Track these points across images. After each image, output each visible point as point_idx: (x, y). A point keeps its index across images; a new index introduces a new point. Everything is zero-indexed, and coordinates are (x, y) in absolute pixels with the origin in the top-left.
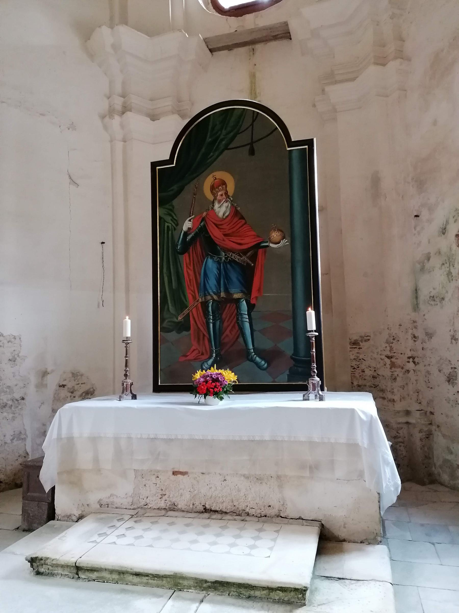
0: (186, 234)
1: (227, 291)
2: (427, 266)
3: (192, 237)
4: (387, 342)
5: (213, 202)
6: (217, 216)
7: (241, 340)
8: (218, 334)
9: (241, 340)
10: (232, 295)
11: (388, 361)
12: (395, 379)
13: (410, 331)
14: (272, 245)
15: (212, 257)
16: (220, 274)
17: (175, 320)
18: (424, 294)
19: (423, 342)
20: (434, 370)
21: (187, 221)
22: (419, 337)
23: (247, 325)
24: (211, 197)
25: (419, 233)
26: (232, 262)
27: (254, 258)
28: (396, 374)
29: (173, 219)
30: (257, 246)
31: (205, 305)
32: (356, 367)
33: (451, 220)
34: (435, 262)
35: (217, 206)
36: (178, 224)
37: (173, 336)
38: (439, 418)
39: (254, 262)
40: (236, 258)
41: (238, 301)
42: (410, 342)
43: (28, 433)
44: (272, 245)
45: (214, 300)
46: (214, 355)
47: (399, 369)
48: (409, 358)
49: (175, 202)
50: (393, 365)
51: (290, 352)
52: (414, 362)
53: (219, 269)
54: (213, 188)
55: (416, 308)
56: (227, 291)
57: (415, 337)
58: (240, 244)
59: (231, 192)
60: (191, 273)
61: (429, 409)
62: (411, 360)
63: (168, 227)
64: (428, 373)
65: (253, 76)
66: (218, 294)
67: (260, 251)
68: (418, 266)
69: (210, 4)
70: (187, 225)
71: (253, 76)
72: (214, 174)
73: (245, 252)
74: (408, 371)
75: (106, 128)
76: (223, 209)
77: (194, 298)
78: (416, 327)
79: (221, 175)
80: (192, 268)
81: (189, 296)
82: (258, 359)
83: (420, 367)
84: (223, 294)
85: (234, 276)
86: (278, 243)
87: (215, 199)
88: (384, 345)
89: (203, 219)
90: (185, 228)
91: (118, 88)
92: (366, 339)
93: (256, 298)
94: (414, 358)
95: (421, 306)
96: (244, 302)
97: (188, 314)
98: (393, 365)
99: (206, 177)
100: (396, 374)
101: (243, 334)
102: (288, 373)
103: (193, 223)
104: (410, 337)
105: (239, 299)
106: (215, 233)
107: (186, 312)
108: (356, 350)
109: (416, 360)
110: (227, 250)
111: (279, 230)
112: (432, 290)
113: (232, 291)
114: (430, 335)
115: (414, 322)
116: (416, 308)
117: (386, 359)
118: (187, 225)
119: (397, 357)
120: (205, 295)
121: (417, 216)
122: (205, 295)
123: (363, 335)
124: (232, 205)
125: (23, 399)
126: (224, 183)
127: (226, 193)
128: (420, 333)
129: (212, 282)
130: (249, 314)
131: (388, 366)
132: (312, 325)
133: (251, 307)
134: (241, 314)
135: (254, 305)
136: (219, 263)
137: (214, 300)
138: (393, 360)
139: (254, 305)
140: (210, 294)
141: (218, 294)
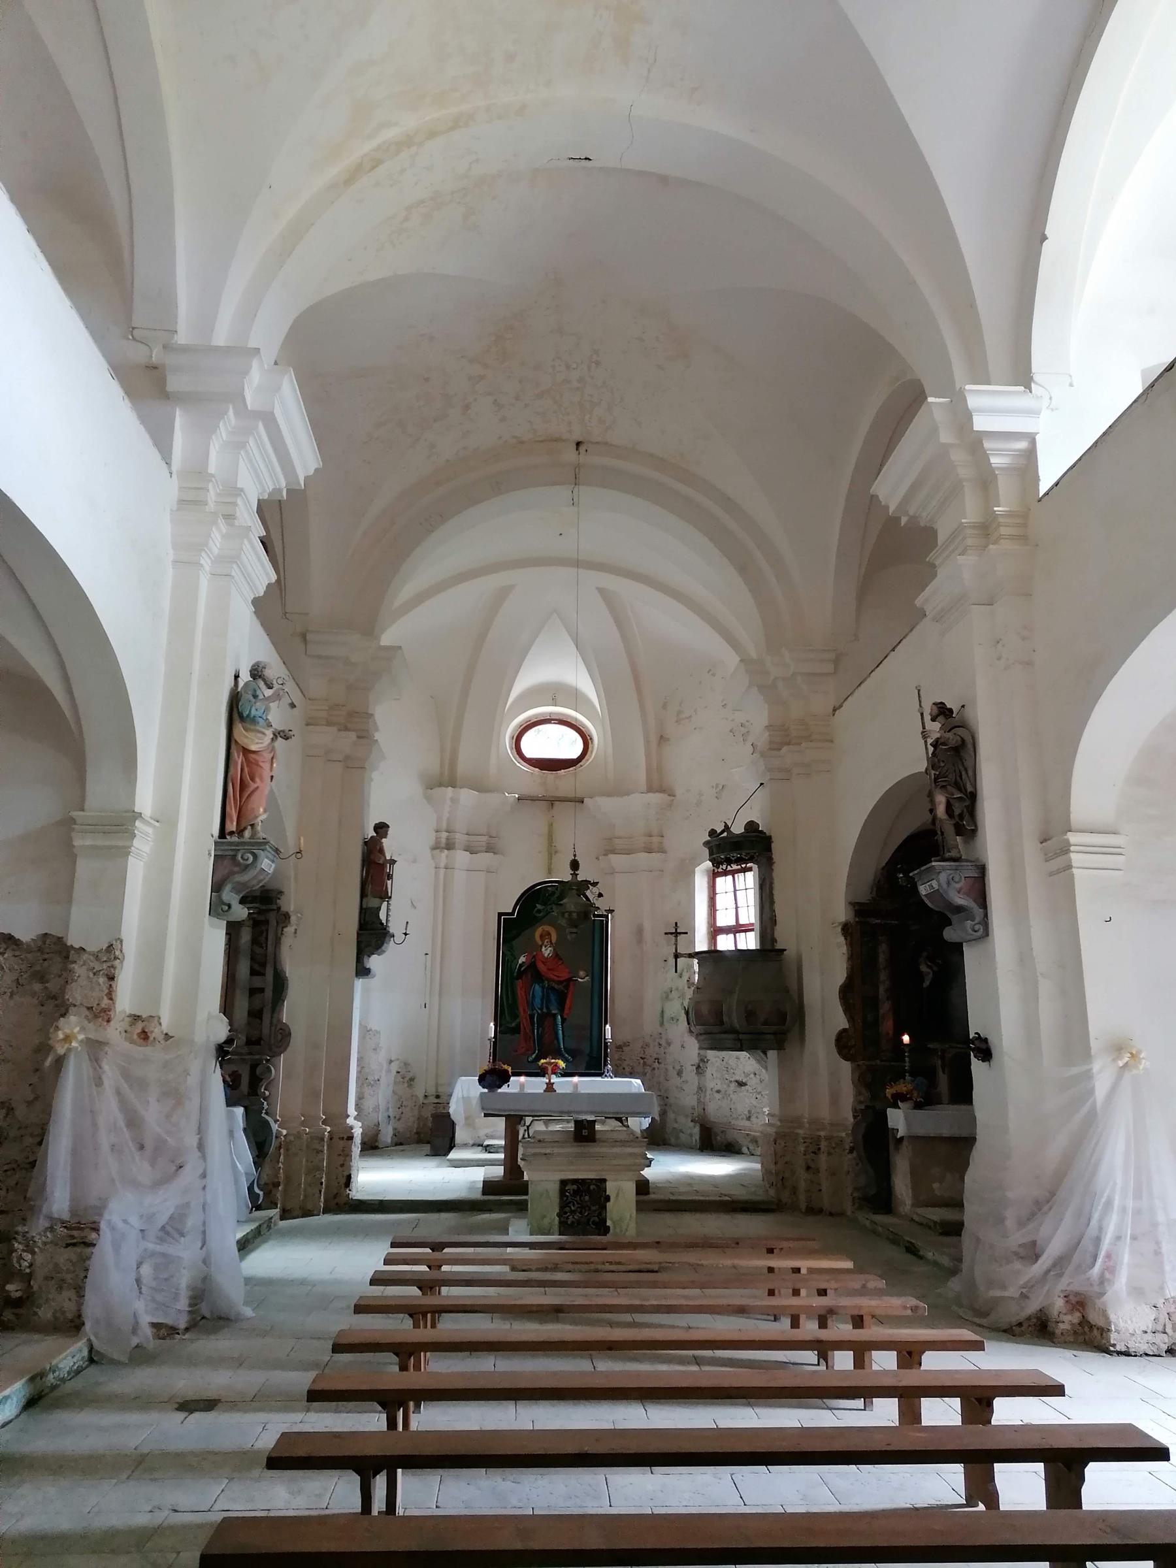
0: (521, 966)
1: (548, 1008)
2: (670, 996)
3: (525, 969)
4: (642, 1047)
5: (541, 946)
6: (544, 956)
7: (556, 1042)
8: (540, 1037)
9: (556, 1042)
10: (551, 1011)
11: (642, 1061)
12: (646, 1074)
13: (657, 1040)
14: (579, 980)
15: (538, 984)
16: (543, 995)
17: (509, 1025)
18: (667, 1015)
19: (665, 1048)
20: (670, 1068)
21: (522, 958)
22: (230, 1072)
23: (560, 1032)
24: (540, 943)
25: (667, 972)
26: (553, 988)
27: (567, 987)
28: (646, 1071)
29: (512, 955)
30: (570, 980)
31: (532, 1017)
32: (618, 1065)
33: (685, 970)
34: (675, 994)
35: (543, 949)
36: (516, 958)
37: (508, 1036)
38: (672, 1100)
39: (567, 989)
40: (556, 986)
41: (555, 1016)
42: (657, 1048)
43: (380, 1107)
44: (579, 980)
45: (538, 1014)
46: (537, 1052)
47: (648, 1067)
48: (655, 1059)
49: (514, 943)
50: (645, 1064)
51: (587, 1051)
52: (658, 1062)
53: (543, 992)
54: (541, 936)
55: (662, 1024)
56: (548, 1008)
57: (660, 1044)
58: (558, 977)
59: (554, 941)
60: (523, 994)
61: (665, 1095)
62: (657, 1061)
63: (508, 960)
64: (666, 1069)
65: (551, 825)
66: (541, 1009)
67: (572, 983)
68: (664, 995)
69: (514, 749)
70: (522, 959)
71: (551, 825)
72: (543, 927)
73: (560, 982)
74: (654, 1069)
75: (433, 857)
76: (548, 952)
77: (524, 1010)
78: (661, 1038)
79: (547, 928)
80: (524, 990)
81: (521, 1010)
82: (566, 1055)
83: (662, 1066)
84: (545, 1010)
85: (553, 997)
86: (584, 978)
87: (543, 944)
88: (640, 1050)
89: (534, 957)
90: (520, 962)
91: (444, 826)
92: (627, 1044)
93: (567, 1014)
94: (658, 1059)
95: (665, 1023)
96: (559, 1016)
97: (520, 1022)
98: (645, 1064)
99: (537, 928)
100: (646, 1071)
101: (558, 1039)
102: (924, 984)
103: (526, 959)
104: (657, 1044)
105: (556, 1014)
106: (541, 967)
107: (518, 1020)
108: (620, 1053)
109: (660, 1061)
110: (549, 980)
111: (585, 970)
112: (672, 1013)
113: (551, 1008)
114: (669, 1044)
115: (661, 1034)
116: (662, 1024)
117: (641, 1060)
118: (522, 959)
119: (951, 876)
120: (533, 1010)
121: (666, 961)
122: (533, 1010)
123: (625, 1041)
124: (554, 949)
125: (379, 1080)
126: (549, 934)
127: (551, 941)
128: (663, 1042)
129: (538, 1001)
130: (562, 1025)
131: (642, 1065)
132: (609, 1035)
133: (563, 1020)
134: (557, 1024)
135: (565, 1019)
136: (543, 988)
137: (538, 1014)
138: (645, 1060)
139: (565, 1019)
140: (535, 1009)
141: (541, 1009)
